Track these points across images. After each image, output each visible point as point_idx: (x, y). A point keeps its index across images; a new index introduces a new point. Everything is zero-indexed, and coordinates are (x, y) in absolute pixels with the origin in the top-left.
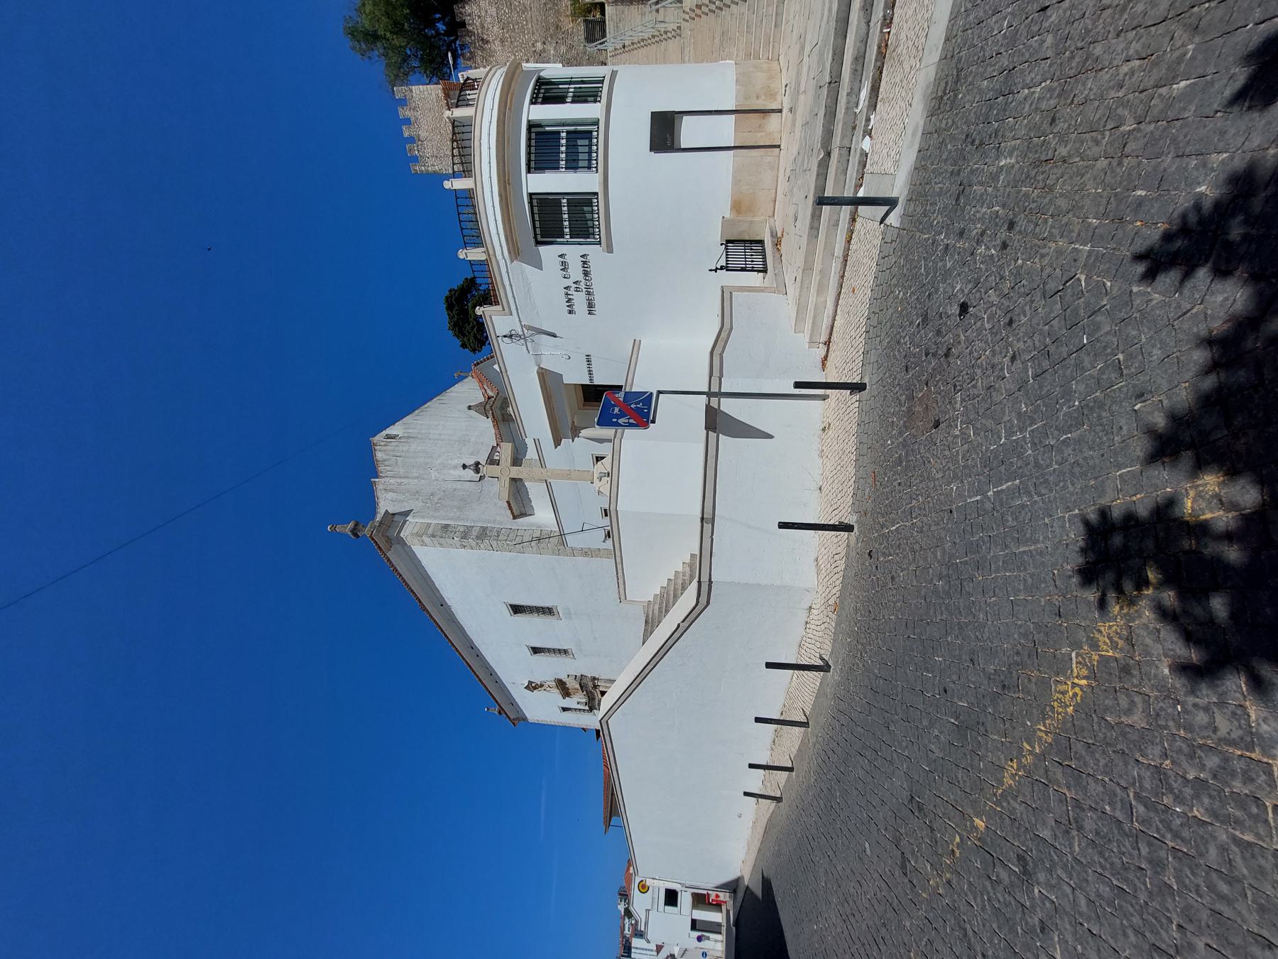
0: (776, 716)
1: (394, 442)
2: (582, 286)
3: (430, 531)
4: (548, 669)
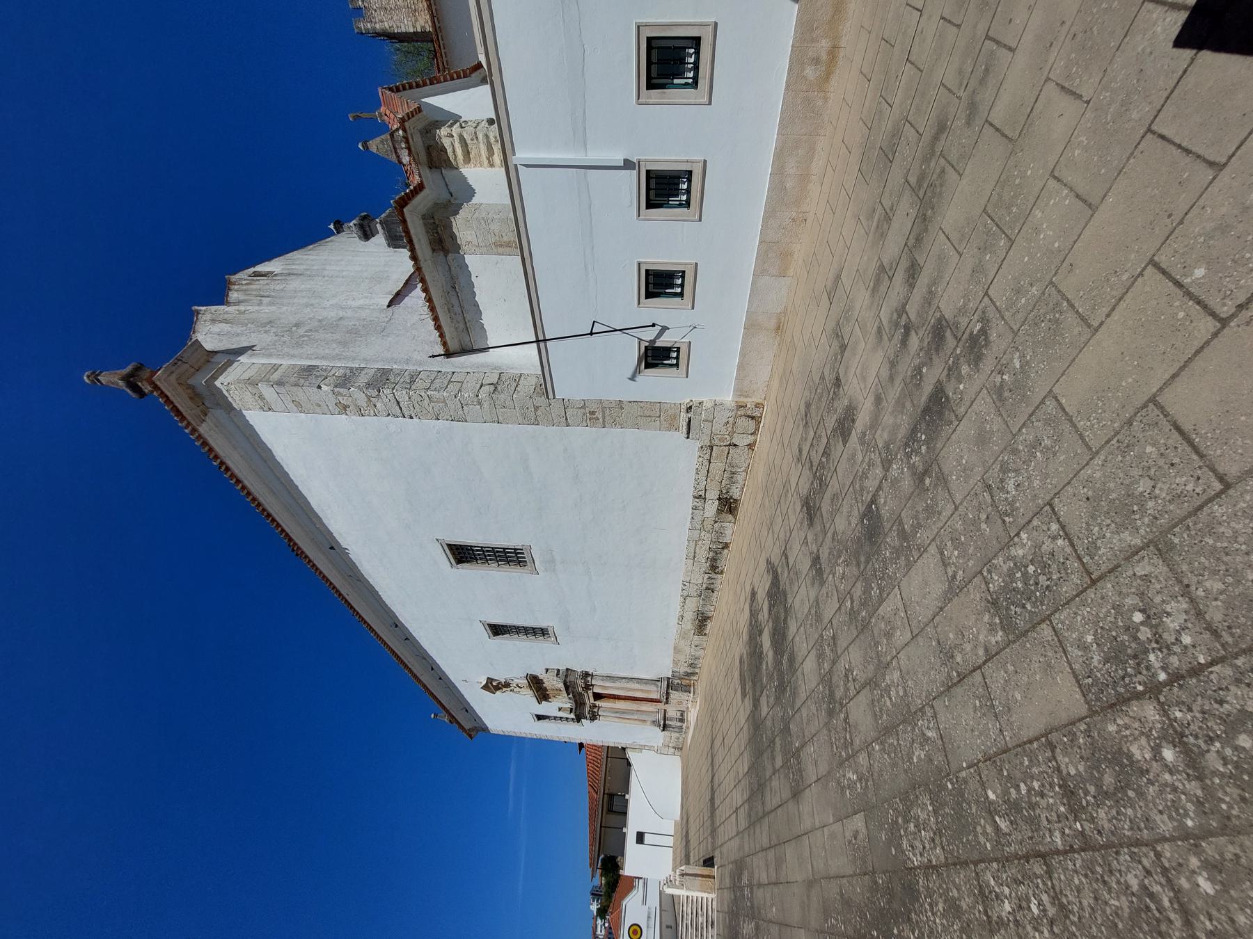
3: (276, 376)
4: (519, 659)
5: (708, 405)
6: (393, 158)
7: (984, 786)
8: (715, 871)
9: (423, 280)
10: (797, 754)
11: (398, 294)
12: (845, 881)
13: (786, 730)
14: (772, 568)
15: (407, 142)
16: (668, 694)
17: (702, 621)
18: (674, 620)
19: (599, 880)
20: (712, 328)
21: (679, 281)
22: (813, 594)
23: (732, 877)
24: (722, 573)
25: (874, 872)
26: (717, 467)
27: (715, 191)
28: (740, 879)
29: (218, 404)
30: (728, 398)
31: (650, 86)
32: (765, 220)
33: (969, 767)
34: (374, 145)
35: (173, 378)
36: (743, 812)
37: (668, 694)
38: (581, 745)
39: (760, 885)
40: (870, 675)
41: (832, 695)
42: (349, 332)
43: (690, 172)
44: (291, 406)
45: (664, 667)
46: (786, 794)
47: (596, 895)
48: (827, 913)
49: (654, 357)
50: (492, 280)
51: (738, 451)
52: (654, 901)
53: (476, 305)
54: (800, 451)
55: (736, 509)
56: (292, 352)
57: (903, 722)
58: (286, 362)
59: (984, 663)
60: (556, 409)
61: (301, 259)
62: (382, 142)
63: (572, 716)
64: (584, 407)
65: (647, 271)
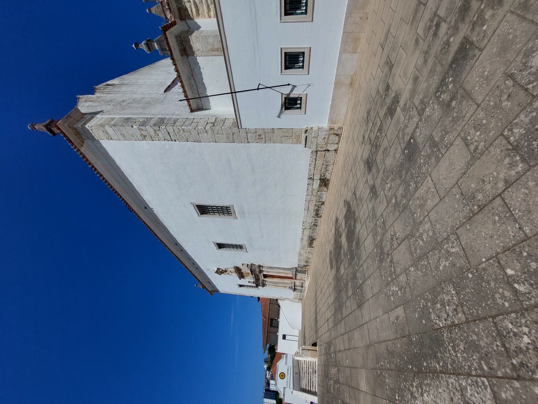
1: (110, 87)
3: (113, 122)
4: (230, 259)
5: (315, 129)
6: (163, 16)
7: (502, 268)
8: (317, 348)
9: (181, 82)
10: (361, 287)
11: (169, 87)
12: (390, 342)
13: (355, 277)
14: (348, 204)
15: (169, 5)
16: (296, 274)
17: (311, 241)
18: (299, 240)
19: (267, 355)
20: (318, 83)
21: (299, 102)
22: (370, 206)
23: (326, 349)
24: (321, 217)
25: (409, 335)
26: (320, 162)
27: (314, 61)
28: (329, 350)
29: (88, 137)
30: (325, 125)
31: (286, 14)
32: (346, 19)
33: (487, 260)
34: (154, 10)
35: (66, 124)
36: (331, 320)
37: (296, 274)
38: (259, 298)
39: (340, 351)
40: (408, 233)
41: (382, 252)
42: (147, 103)
43: (304, 53)
44: (121, 137)
45: (293, 262)
46: (354, 306)
47: (266, 362)
48: (378, 360)
49: (289, 104)
50: (210, 68)
51: (330, 153)
52: (290, 363)
53: (204, 84)
54: (364, 137)
55: (328, 184)
56: (120, 112)
57: (432, 250)
58: (117, 117)
59: (504, 191)
60: (243, 133)
61: (127, 78)
62: (157, 7)
63: (254, 285)
64: (255, 132)
65: (285, 53)
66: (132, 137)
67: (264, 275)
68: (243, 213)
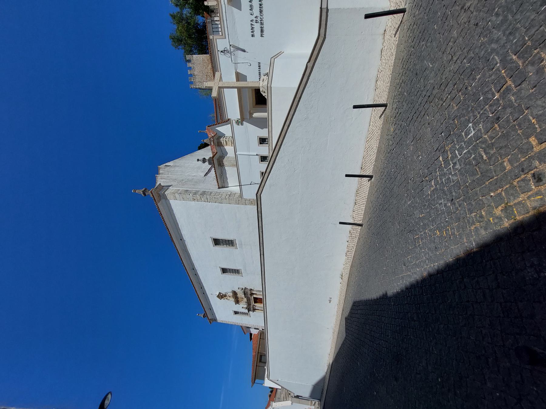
0: (351, 221)
2: (259, 19)
3: (179, 192)
50: (230, 172)
58: (181, 189)
61: (178, 162)
66: (188, 199)
67: (254, 298)
68: (241, 245)
